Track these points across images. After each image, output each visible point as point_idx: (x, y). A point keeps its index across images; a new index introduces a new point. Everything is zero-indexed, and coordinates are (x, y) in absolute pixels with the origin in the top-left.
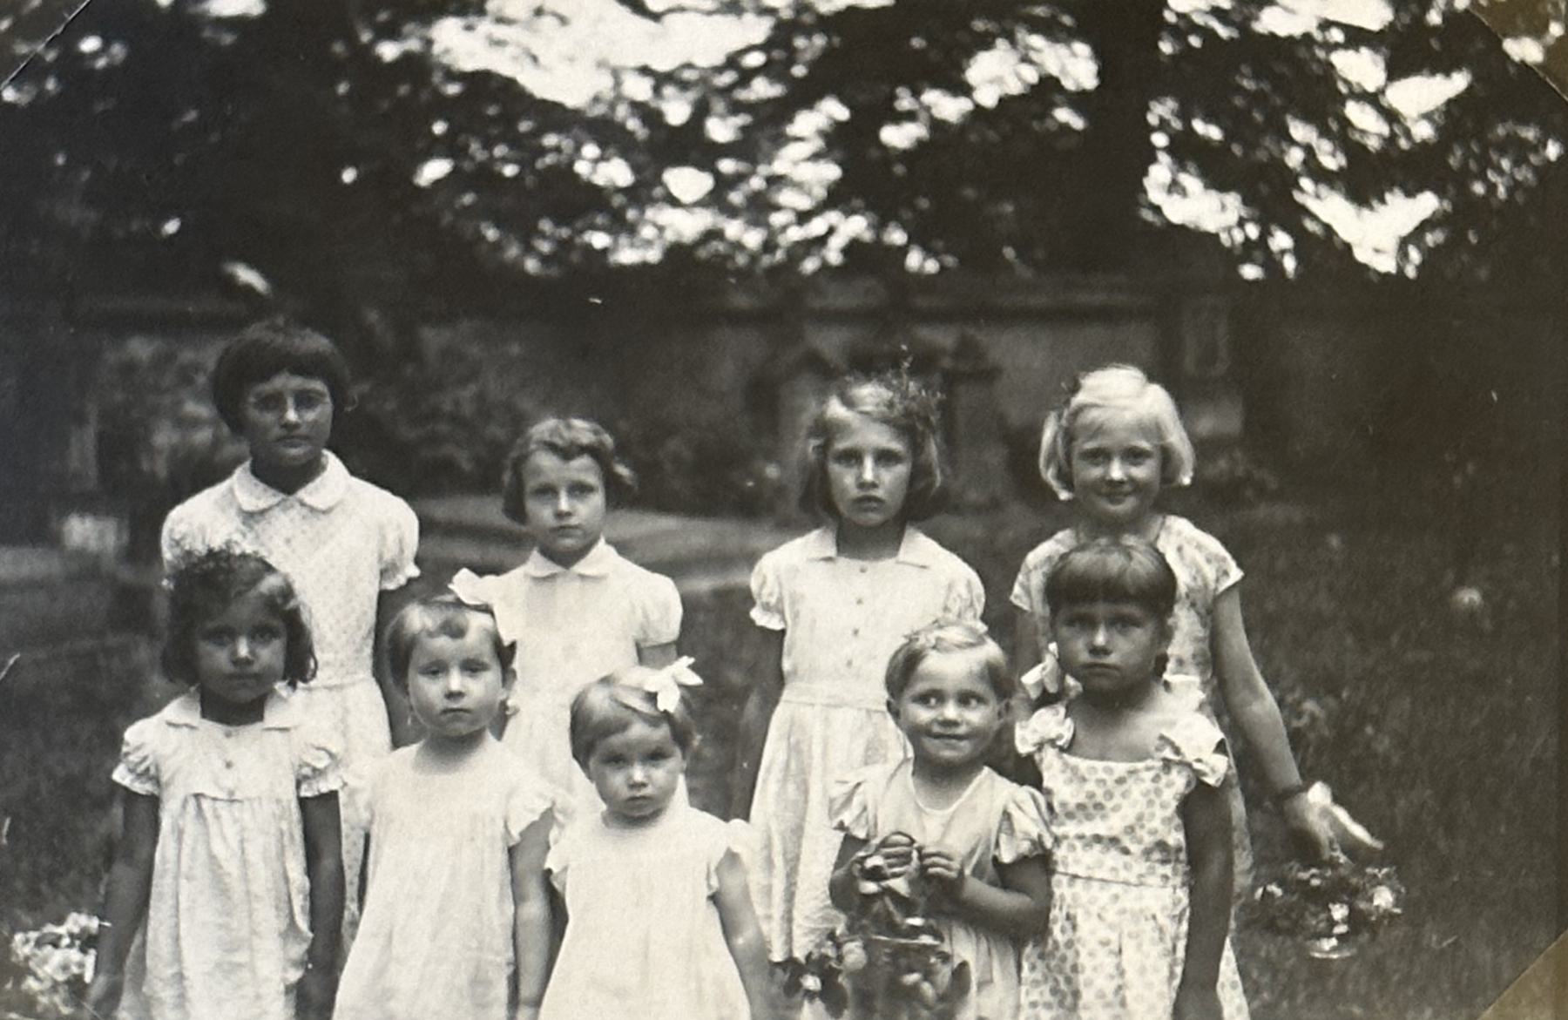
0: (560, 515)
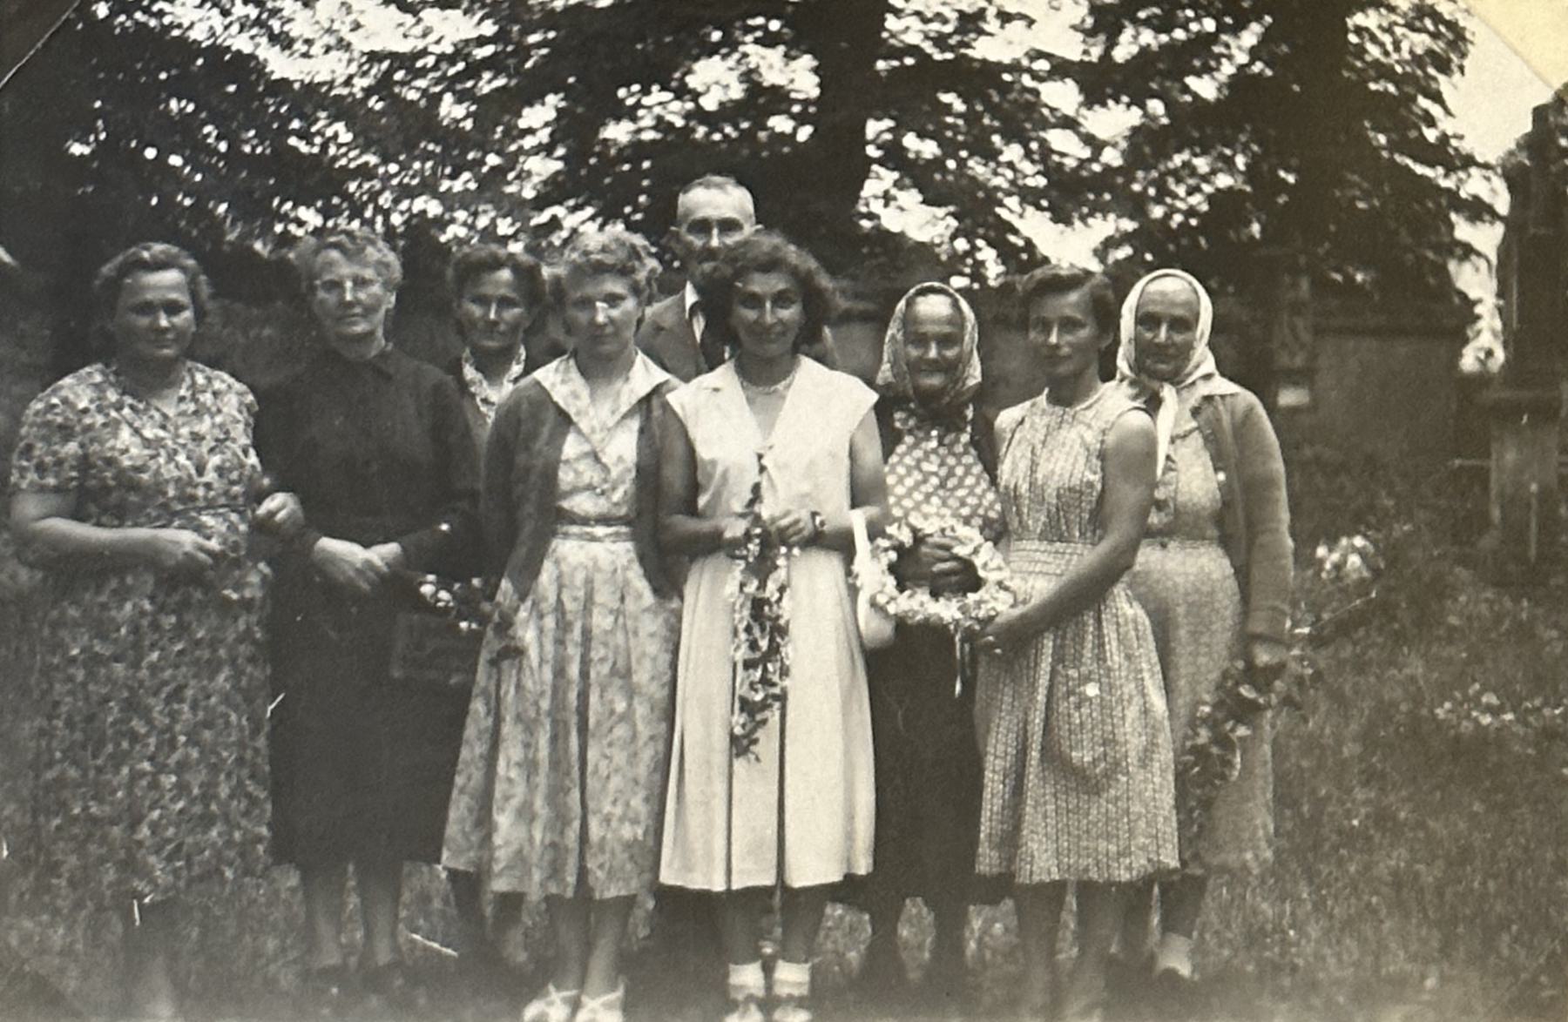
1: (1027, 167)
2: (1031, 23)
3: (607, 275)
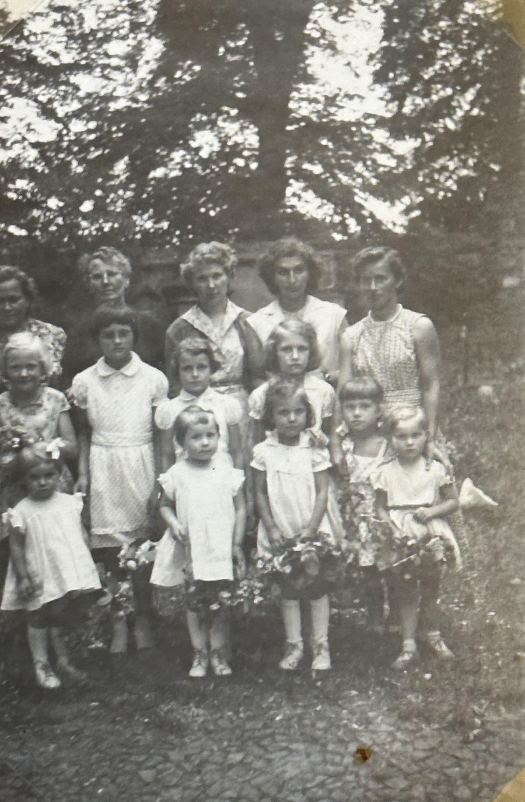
0: (195, 377)
1: (367, 174)
2: (361, 97)
3: (212, 265)
